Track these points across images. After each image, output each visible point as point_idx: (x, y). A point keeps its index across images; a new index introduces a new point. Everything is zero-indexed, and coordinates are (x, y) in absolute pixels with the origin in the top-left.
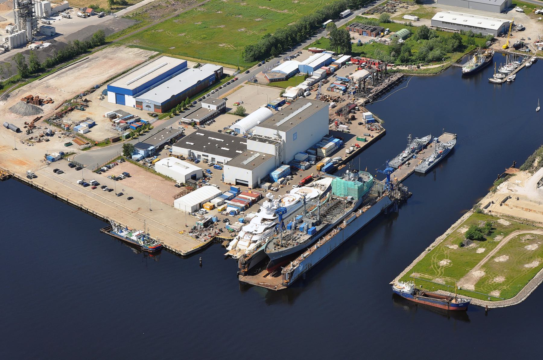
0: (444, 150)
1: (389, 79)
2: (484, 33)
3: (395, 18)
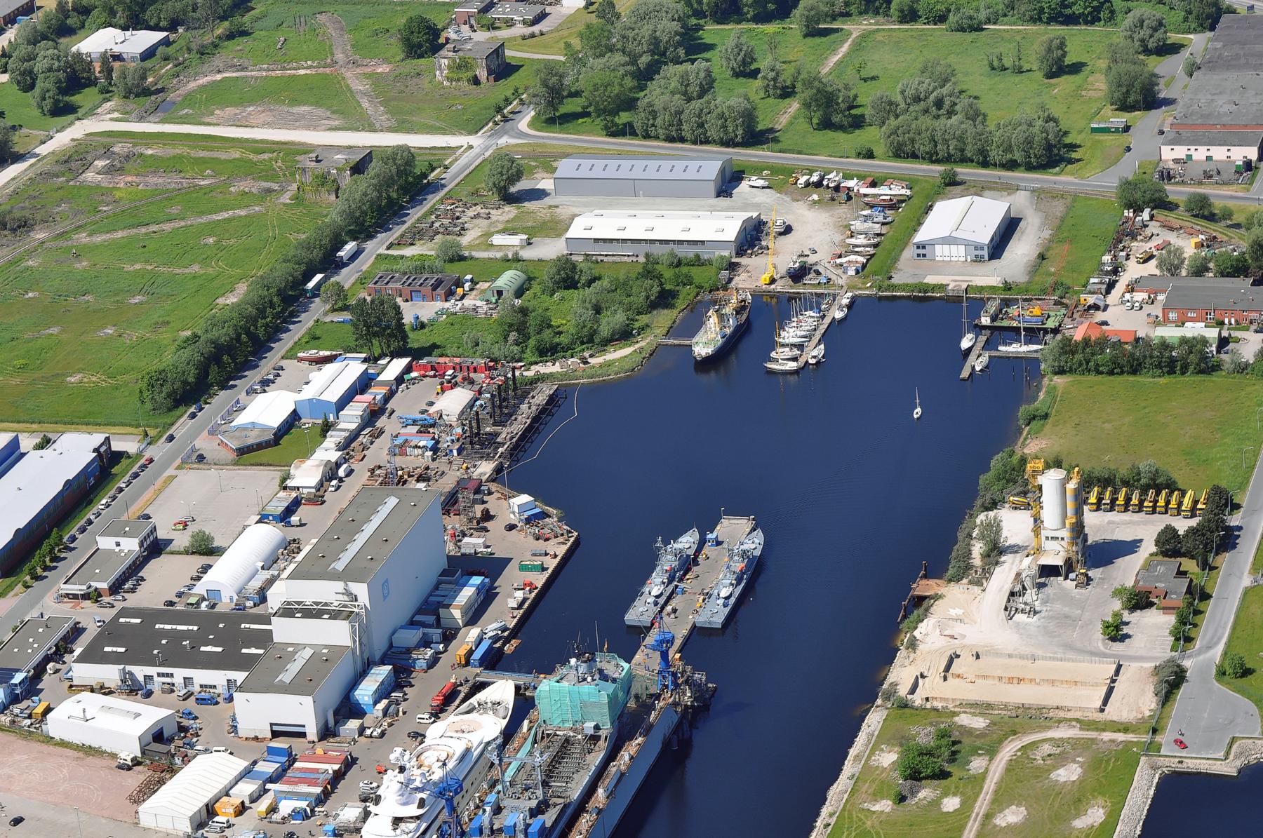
0: (746, 561)
1: (529, 403)
3: (471, 247)
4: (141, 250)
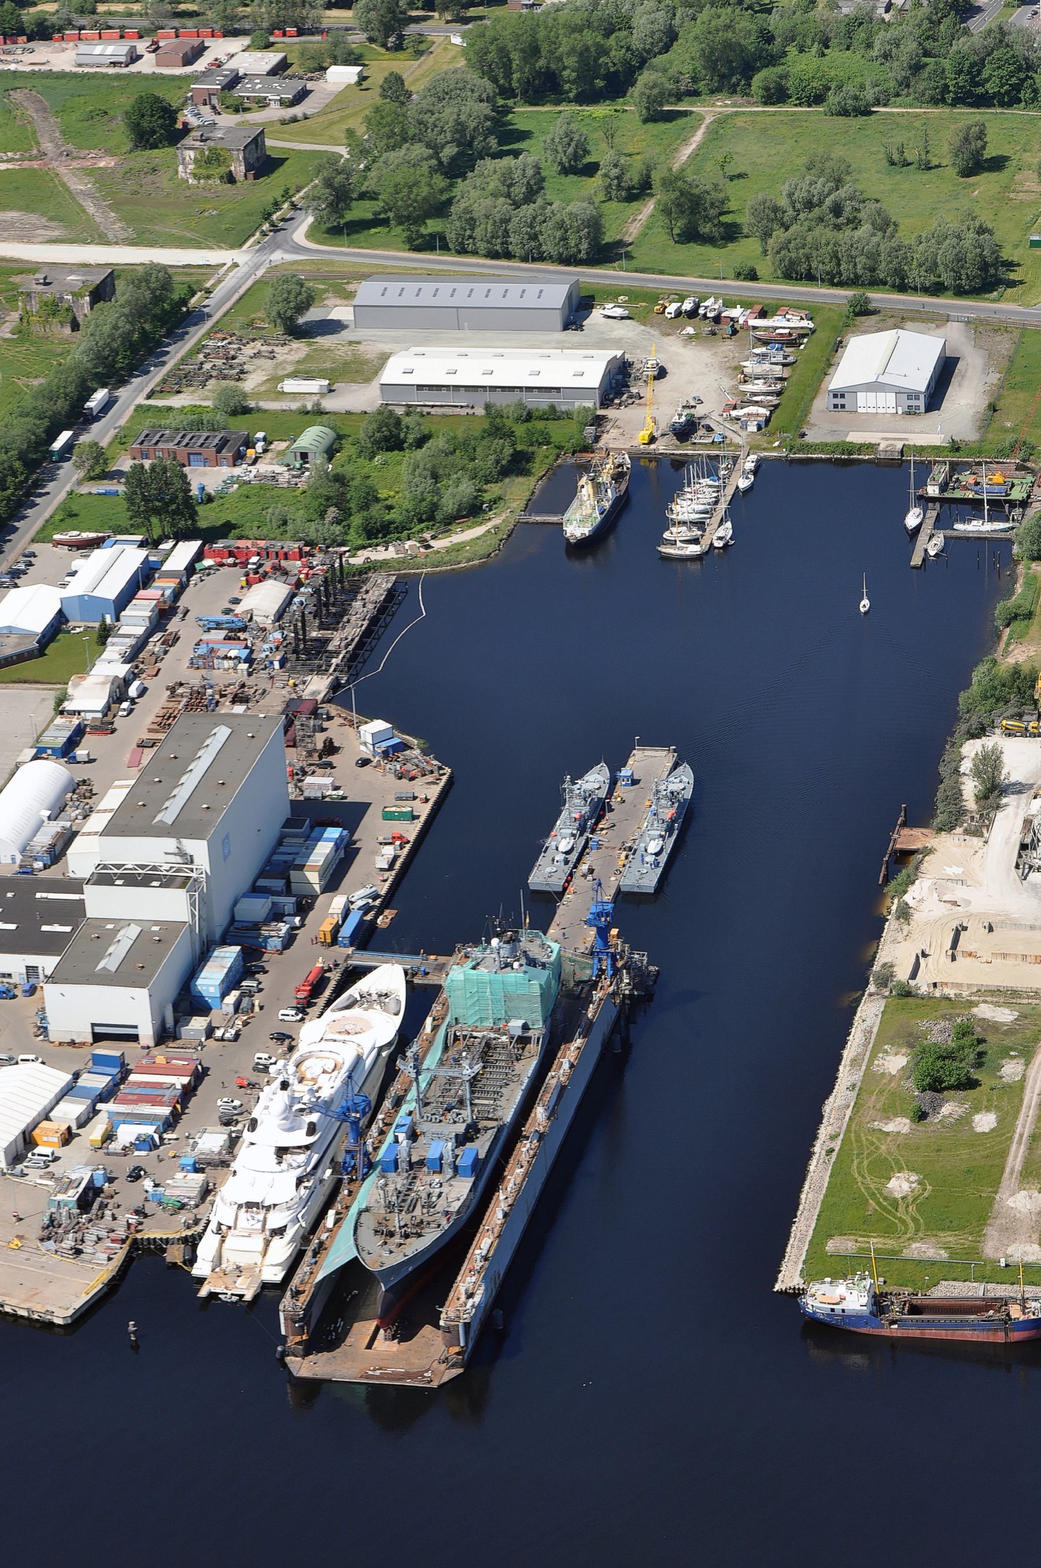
0: (676, 805)
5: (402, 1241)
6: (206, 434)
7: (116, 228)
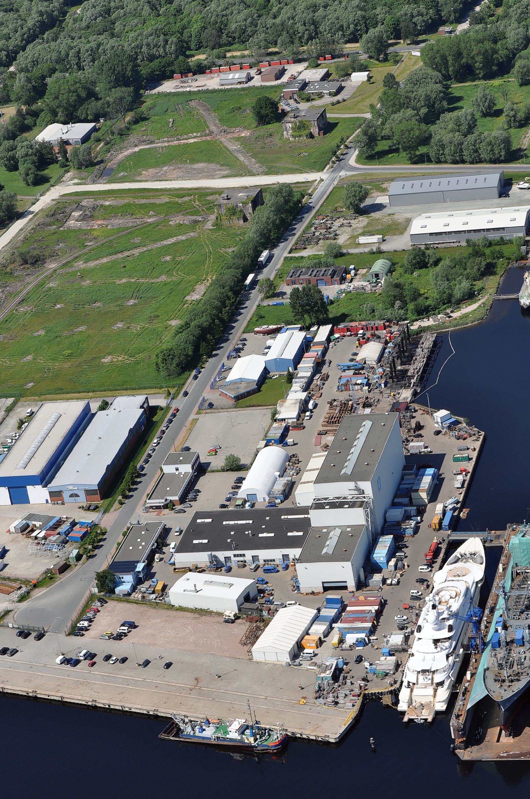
2: (507, 237)
4: (123, 269)
5: (510, 684)
6: (324, 269)
7: (257, 168)
